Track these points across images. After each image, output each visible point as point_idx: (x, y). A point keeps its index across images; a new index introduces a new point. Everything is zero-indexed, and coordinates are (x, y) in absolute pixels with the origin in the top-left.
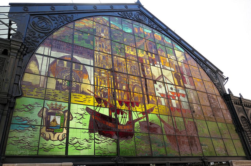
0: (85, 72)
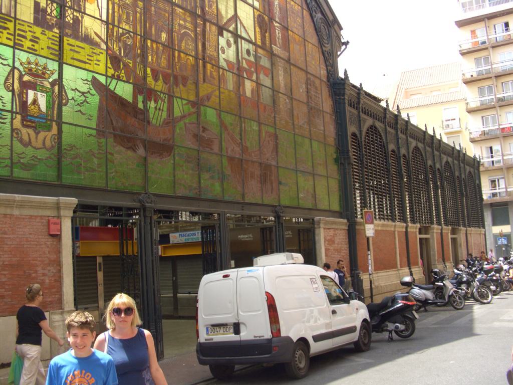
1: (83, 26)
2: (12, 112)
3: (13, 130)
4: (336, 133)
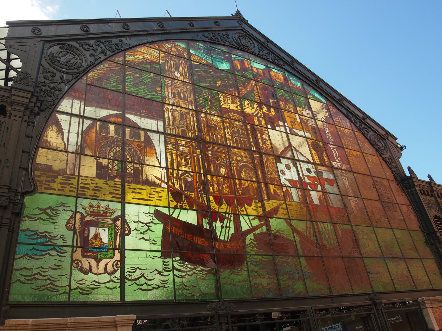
0: (149, 142)
1: (144, 173)
2: (72, 247)
3: (72, 261)
4: (418, 220)
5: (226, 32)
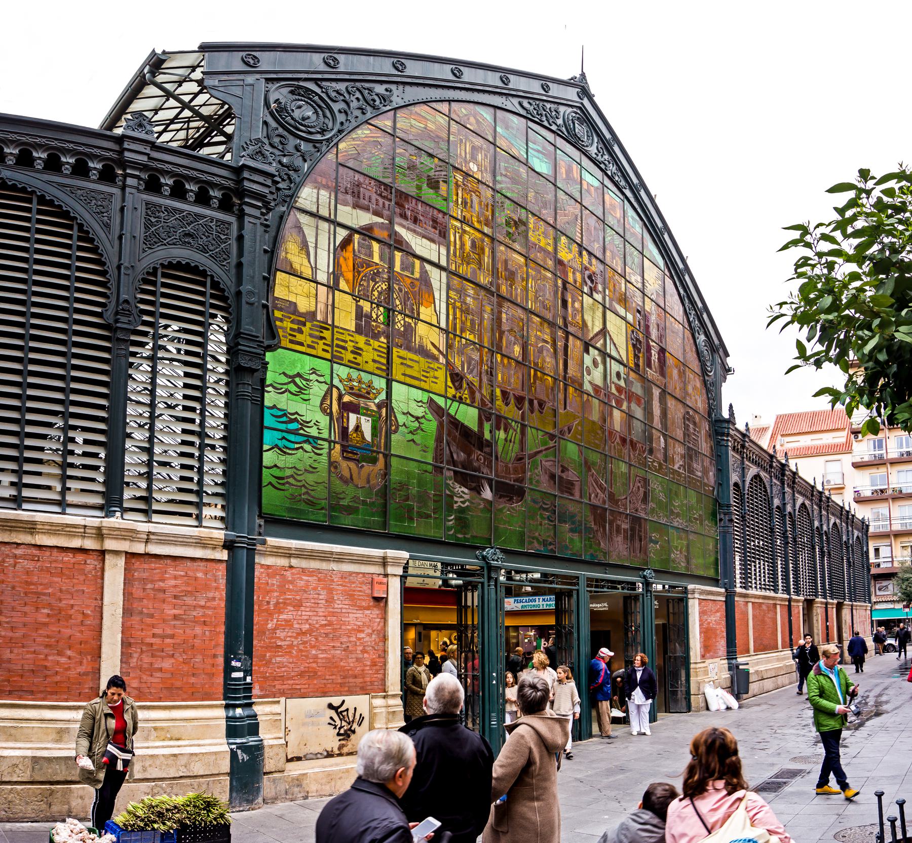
0: (425, 280)
5: (556, 106)
